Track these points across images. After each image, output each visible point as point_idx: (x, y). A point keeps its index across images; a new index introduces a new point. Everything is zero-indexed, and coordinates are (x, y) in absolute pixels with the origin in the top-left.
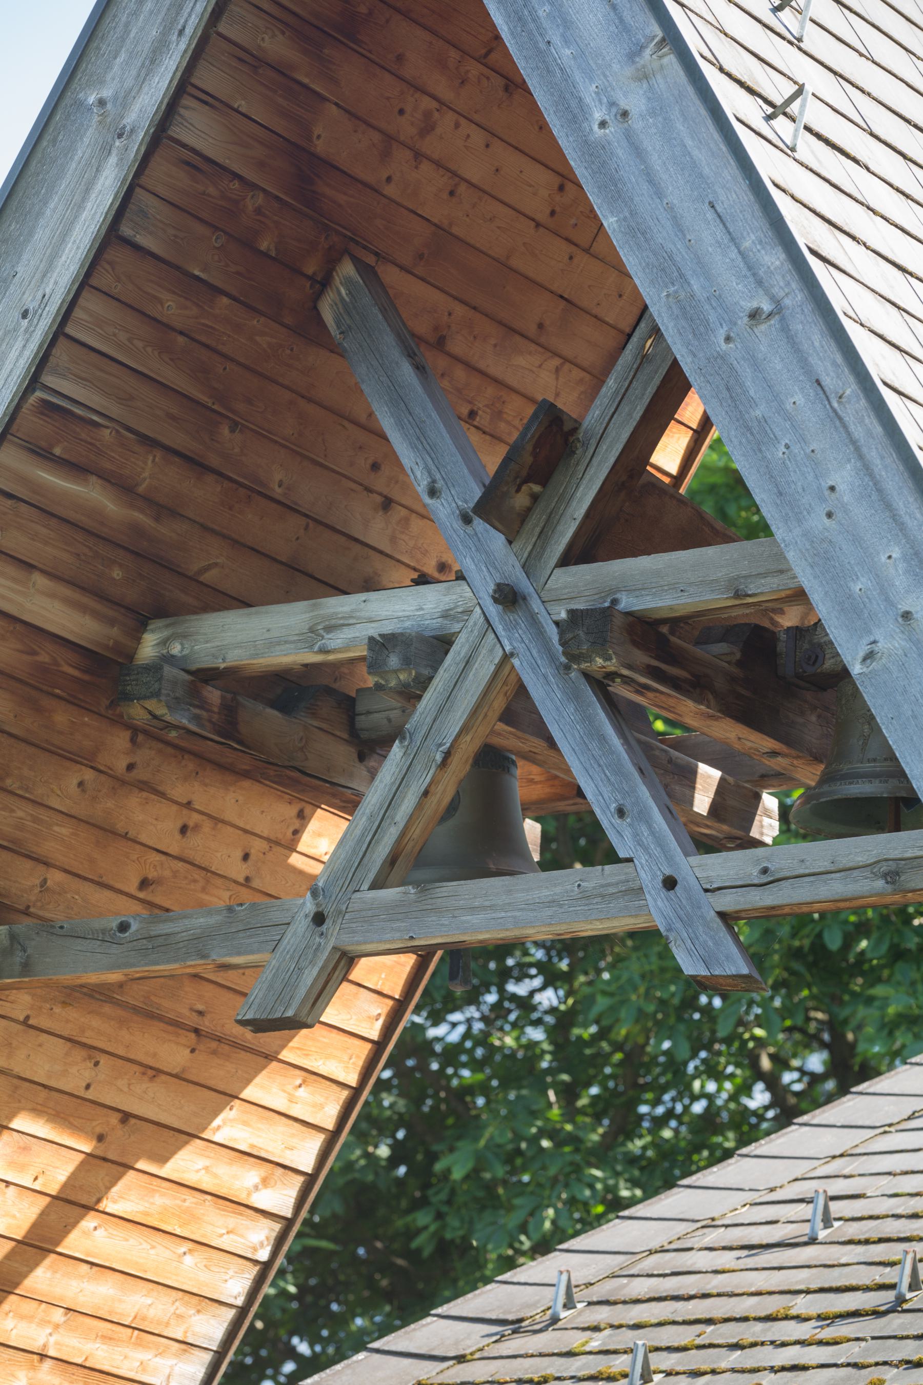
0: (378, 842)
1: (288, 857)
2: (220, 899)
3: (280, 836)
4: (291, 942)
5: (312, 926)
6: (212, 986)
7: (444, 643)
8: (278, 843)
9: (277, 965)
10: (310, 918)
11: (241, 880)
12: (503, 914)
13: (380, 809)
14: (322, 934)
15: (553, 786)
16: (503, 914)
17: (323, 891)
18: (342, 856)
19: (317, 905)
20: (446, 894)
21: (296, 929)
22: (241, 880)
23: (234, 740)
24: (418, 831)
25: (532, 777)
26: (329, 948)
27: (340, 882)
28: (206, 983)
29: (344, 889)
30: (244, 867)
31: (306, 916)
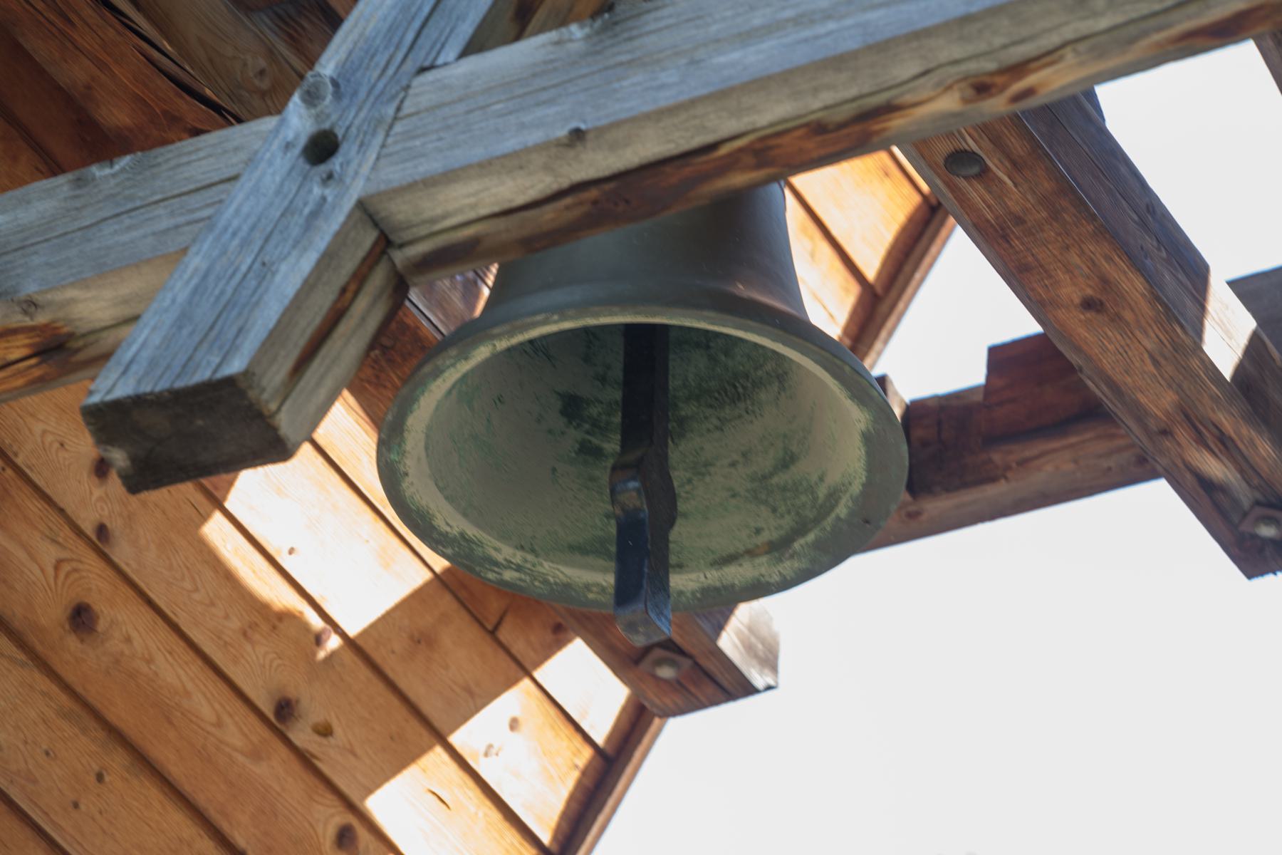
1: (205, 518)
2: (32, 557)
4: (245, 209)
9: (204, 266)
10: (297, 151)
11: (89, 529)
12: (831, 26)
14: (330, 176)
17: (335, 83)
20: (671, 21)
26: (348, 204)
27: (381, 59)
29: (390, 71)
30: (98, 492)
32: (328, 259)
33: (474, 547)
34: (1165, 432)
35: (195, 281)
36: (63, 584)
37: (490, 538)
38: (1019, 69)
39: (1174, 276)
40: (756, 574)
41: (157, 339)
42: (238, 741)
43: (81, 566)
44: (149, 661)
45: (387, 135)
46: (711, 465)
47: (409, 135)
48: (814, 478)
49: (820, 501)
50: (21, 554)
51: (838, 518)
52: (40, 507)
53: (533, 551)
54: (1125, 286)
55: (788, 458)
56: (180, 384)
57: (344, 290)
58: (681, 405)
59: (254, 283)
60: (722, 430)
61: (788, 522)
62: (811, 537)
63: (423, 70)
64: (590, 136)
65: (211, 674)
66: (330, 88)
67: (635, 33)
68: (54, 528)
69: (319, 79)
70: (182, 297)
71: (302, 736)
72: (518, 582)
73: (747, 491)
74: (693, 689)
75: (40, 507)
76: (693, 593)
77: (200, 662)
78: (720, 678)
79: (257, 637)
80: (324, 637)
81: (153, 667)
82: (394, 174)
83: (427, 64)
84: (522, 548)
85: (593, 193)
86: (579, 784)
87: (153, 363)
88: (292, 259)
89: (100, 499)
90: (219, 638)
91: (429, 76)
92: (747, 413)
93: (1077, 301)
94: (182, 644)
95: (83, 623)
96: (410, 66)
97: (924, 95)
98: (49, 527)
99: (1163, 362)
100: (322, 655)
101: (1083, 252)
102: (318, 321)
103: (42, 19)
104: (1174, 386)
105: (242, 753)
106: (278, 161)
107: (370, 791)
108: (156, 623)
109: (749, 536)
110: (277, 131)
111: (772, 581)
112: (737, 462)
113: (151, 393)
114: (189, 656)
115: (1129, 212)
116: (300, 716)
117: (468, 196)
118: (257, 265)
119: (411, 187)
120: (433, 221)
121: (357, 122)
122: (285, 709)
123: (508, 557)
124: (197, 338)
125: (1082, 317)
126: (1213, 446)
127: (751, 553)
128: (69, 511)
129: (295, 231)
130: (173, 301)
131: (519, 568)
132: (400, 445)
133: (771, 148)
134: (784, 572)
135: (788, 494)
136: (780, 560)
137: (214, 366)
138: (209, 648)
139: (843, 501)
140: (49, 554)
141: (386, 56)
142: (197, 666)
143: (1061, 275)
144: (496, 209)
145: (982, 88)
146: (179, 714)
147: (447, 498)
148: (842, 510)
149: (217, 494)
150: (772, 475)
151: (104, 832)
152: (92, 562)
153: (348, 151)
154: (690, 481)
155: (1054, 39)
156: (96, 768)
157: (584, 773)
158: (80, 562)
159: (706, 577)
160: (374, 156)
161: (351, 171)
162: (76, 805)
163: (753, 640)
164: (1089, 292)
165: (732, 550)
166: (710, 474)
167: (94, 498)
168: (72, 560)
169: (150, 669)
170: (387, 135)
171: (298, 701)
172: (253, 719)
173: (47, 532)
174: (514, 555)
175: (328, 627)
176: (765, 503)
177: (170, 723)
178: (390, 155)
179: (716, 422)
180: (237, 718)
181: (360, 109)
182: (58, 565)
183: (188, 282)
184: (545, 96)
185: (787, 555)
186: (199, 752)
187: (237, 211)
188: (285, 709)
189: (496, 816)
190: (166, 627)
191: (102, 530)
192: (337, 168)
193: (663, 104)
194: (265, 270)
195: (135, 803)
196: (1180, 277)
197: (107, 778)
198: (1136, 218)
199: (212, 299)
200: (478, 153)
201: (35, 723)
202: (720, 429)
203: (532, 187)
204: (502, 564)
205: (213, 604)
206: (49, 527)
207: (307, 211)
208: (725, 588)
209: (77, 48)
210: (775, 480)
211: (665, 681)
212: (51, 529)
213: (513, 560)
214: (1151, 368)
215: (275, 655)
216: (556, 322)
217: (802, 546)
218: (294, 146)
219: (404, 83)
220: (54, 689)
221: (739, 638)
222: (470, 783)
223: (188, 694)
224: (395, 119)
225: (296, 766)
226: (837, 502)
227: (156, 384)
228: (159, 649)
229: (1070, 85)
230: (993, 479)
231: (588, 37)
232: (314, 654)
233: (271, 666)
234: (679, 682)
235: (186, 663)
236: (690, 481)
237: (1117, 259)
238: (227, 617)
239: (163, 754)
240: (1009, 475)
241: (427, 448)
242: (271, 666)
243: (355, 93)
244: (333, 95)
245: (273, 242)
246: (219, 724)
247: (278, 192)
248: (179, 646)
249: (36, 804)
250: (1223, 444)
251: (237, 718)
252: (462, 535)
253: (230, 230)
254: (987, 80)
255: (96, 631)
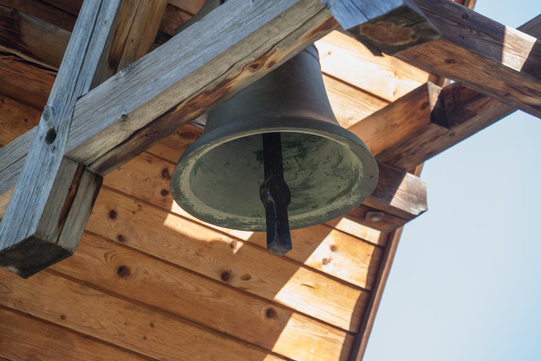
0: (93, 46)
1: (165, 219)
2: (93, 256)
3: (147, 195)
4: (30, 167)
5: (46, 145)
6: (109, 349)
8: (147, 202)
9: (20, 193)
10: (44, 139)
11: (114, 238)
12: (194, 57)
13: (93, 16)
14: (54, 148)
15: (411, 122)
16: (194, 58)
17: (53, 109)
18: (66, 72)
19: (49, 125)
20: (149, 64)
21: (34, 153)
22: (114, 238)
23: (18, 49)
24: (135, 32)
25: (394, 122)
26: (60, 158)
27: (66, 96)
28: (100, 345)
29: (69, 101)
30: (113, 225)
31: (41, 138)
32: (58, 181)
33: (235, 221)
34: (507, 94)
35: (18, 199)
36: (110, 262)
37: (239, 216)
38: (263, 57)
39: (482, 39)
40: (344, 203)
41: (8, 225)
42: (209, 293)
43: (116, 253)
44: (159, 277)
45: (70, 128)
46: (318, 165)
47: (77, 126)
48: (349, 164)
49: (354, 172)
50: (88, 257)
51: (361, 178)
52: (90, 237)
53: (259, 216)
54: (458, 52)
55: (340, 158)
56: (16, 242)
57: (70, 189)
58: (303, 143)
59: (35, 196)
60: (318, 151)
61: (347, 182)
62: (356, 186)
63: (79, 98)
64: (129, 116)
65: (187, 273)
66: (52, 112)
67: (138, 71)
68: (99, 243)
69: (48, 108)
70: (14, 207)
71: (236, 283)
72: (258, 228)
73: (332, 172)
74: (392, 221)
75: (90, 237)
76: (325, 215)
77: (181, 271)
78: (399, 215)
79: (203, 254)
80: (234, 244)
81: (161, 279)
82: (73, 143)
83: (79, 96)
84: (254, 216)
85: (143, 133)
86: (372, 261)
87: (8, 235)
88: (46, 184)
89: (116, 226)
90: (187, 259)
91: (81, 100)
92: (325, 142)
93: (444, 62)
94: (171, 267)
95: (124, 273)
96: (74, 98)
97: (236, 73)
98: (96, 243)
99: (490, 72)
100: (235, 251)
101: (434, 46)
102: (63, 204)
103: (11, 74)
104: (500, 79)
105: (212, 297)
106: (39, 145)
107: (275, 293)
108: (156, 263)
109: (337, 190)
110: (37, 132)
111: (351, 204)
112: (326, 162)
113: (8, 248)
114: (176, 270)
115: (452, 23)
116: (233, 276)
117: (101, 145)
118: (36, 189)
119: (79, 147)
120: (94, 155)
121: (61, 124)
122: (226, 276)
123: (250, 221)
124: (20, 222)
125: (449, 66)
126: (529, 94)
127: (340, 196)
128: (103, 235)
129: (46, 172)
130: (12, 208)
131: (256, 223)
132: (183, 197)
133: (195, 103)
134: (354, 200)
135: (344, 171)
136: (350, 197)
137: (26, 233)
138: (183, 265)
139: (360, 172)
140: (101, 253)
141: (67, 95)
142: (180, 273)
143: (431, 55)
144: (114, 146)
145: (255, 67)
146: (178, 292)
147: (215, 208)
148: (361, 175)
149: (167, 208)
150: (337, 165)
151: (161, 344)
152: (120, 251)
153: (59, 136)
154: (312, 173)
155: (268, 46)
156: (149, 322)
157: (373, 256)
158: (115, 251)
159: (327, 209)
160: (67, 137)
161: (60, 144)
162: (145, 338)
163: (411, 195)
164: (446, 57)
165: (333, 197)
166: (318, 169)
167: (113, 227)
168: (111, 252)
169: (160, 280)
170: (70, 128)
171: (231, 271)
172: (212, 284)
173: (97, 245)
174: (252, 219)
175: (234, 240)
176: (338, 176)
177: (176, 296)
178: (71, 136)
179: (315, 147)
180: (205, 286)
181: (61, 118)
182: (106, 256)
183: (16, 200)
184: (114, 102)
185: (351, 194)
186: (193, 303)
187: (28, 168)
188: (226, 276)
189: (337, 285)
190: (162, 263)
191: (120, 238)
192: (56, 144)
193: (148, 100)
194: (38, 189)
195: (171, 330)
196: (486, 38)
197: (155, 325)
198: (456, 24)
199: (24, 206)
200: (96, 130)
201: (117, 315)
202: (317, 150)
203: (121, 136)
204: (249, 224)
205: (179, 248)
206: (96, 243)
207: (49, 163)
208: (336, 210)
209: (29, 79)
210: (339, 167)
211: (377, 222)
212: (98, 244)
213: (252, 221)
214: (487, 75)
215: (214, 258)
216: (209, 146)
217: (355, 190)
218: (43, 138)
219: (73, 105)
220: (120, 300)
221: (403, 198)
222: (321, 276)
223: (180, 284)
224: (72, 120)
225: (238, 295)
226: (358, 174)
227: (9, 244)
228: (161, 272)
229: (286, 57)
230: (475, 115)
231: (125, 75)
232: (232, 252)
233: (214, 262)
234: (383, 220)
235: (175, 273)
236: (312, 173)
237: (448, 44)
238: (188, 251)
239: (174, 308)
240: (478, 112)
241: (196, 195)
242: (214, 262)
243: (59, 112)
244: (53, 114)
245: (39, 179)
246: (198, 290)
247: (40, 157)
248: (171, 268)
249: (127, 343)
250: (532, 92)
251: (205, 286)
252: (228, 218)
253: (27, 176)
254: (256, 63)
255: (131, 274)
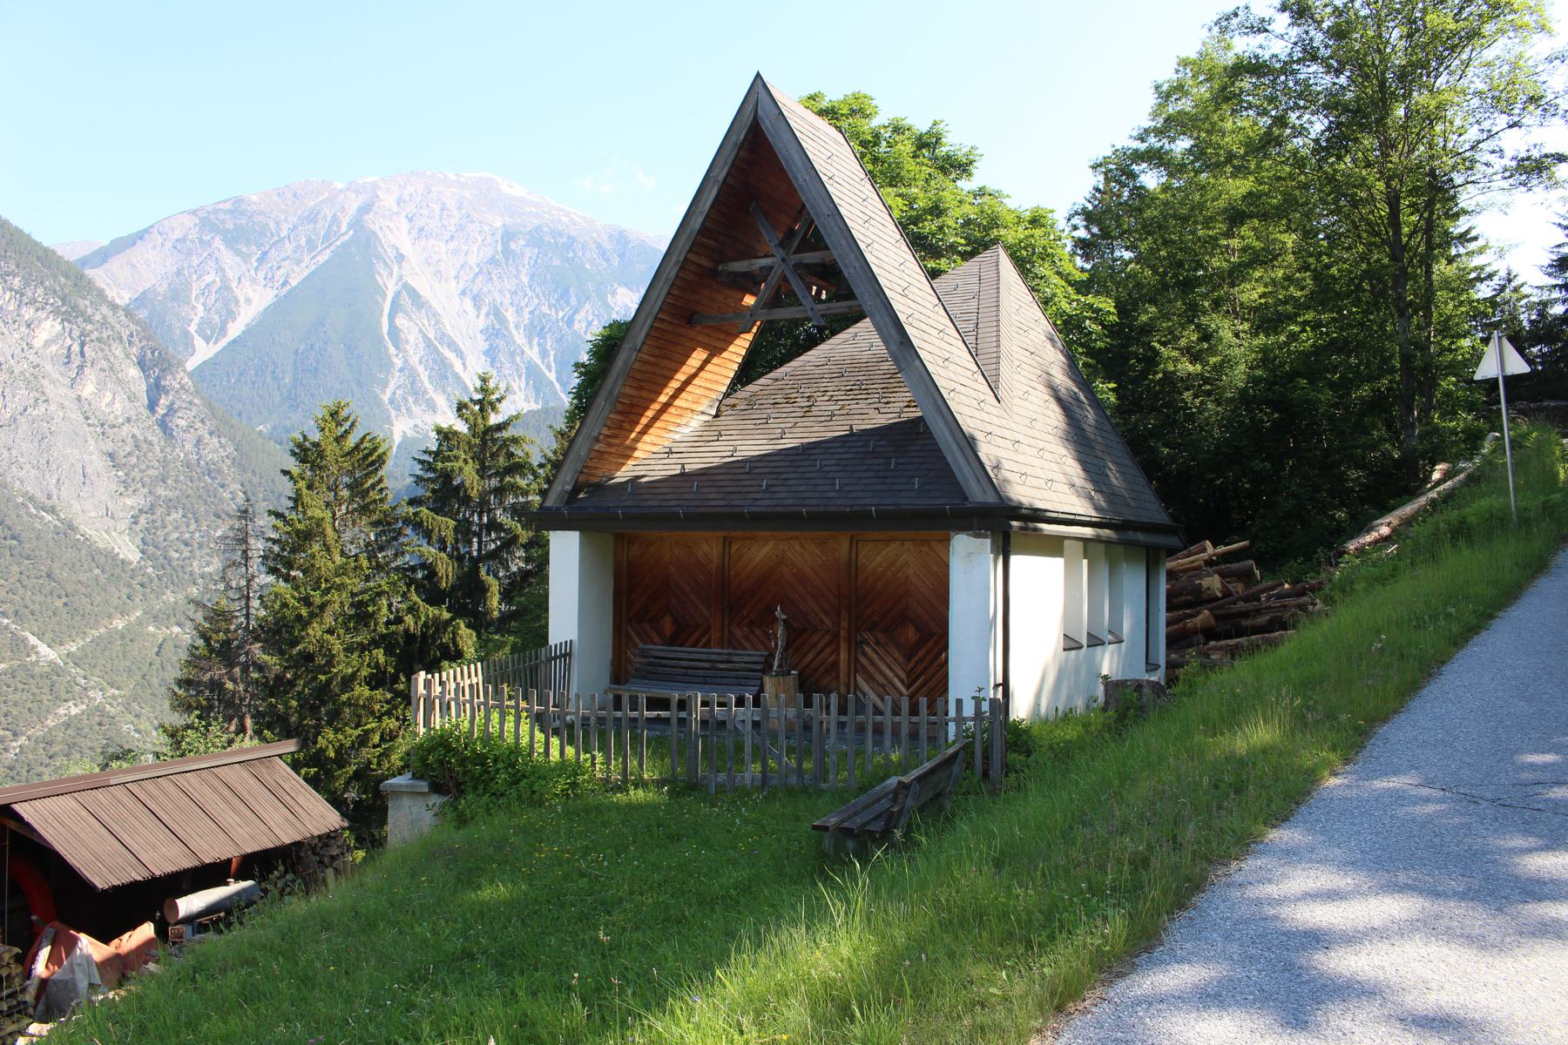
7: (772, 268)
